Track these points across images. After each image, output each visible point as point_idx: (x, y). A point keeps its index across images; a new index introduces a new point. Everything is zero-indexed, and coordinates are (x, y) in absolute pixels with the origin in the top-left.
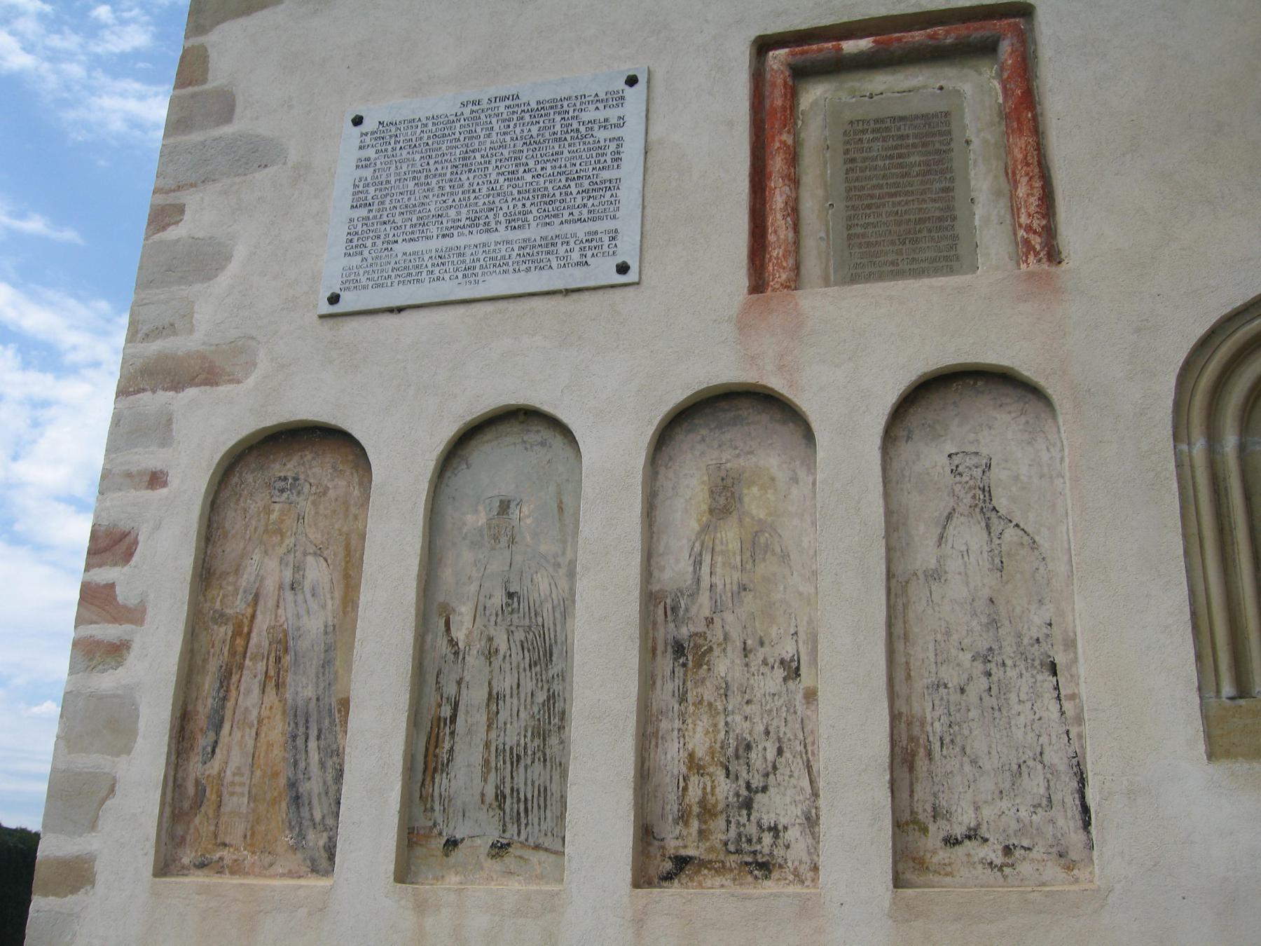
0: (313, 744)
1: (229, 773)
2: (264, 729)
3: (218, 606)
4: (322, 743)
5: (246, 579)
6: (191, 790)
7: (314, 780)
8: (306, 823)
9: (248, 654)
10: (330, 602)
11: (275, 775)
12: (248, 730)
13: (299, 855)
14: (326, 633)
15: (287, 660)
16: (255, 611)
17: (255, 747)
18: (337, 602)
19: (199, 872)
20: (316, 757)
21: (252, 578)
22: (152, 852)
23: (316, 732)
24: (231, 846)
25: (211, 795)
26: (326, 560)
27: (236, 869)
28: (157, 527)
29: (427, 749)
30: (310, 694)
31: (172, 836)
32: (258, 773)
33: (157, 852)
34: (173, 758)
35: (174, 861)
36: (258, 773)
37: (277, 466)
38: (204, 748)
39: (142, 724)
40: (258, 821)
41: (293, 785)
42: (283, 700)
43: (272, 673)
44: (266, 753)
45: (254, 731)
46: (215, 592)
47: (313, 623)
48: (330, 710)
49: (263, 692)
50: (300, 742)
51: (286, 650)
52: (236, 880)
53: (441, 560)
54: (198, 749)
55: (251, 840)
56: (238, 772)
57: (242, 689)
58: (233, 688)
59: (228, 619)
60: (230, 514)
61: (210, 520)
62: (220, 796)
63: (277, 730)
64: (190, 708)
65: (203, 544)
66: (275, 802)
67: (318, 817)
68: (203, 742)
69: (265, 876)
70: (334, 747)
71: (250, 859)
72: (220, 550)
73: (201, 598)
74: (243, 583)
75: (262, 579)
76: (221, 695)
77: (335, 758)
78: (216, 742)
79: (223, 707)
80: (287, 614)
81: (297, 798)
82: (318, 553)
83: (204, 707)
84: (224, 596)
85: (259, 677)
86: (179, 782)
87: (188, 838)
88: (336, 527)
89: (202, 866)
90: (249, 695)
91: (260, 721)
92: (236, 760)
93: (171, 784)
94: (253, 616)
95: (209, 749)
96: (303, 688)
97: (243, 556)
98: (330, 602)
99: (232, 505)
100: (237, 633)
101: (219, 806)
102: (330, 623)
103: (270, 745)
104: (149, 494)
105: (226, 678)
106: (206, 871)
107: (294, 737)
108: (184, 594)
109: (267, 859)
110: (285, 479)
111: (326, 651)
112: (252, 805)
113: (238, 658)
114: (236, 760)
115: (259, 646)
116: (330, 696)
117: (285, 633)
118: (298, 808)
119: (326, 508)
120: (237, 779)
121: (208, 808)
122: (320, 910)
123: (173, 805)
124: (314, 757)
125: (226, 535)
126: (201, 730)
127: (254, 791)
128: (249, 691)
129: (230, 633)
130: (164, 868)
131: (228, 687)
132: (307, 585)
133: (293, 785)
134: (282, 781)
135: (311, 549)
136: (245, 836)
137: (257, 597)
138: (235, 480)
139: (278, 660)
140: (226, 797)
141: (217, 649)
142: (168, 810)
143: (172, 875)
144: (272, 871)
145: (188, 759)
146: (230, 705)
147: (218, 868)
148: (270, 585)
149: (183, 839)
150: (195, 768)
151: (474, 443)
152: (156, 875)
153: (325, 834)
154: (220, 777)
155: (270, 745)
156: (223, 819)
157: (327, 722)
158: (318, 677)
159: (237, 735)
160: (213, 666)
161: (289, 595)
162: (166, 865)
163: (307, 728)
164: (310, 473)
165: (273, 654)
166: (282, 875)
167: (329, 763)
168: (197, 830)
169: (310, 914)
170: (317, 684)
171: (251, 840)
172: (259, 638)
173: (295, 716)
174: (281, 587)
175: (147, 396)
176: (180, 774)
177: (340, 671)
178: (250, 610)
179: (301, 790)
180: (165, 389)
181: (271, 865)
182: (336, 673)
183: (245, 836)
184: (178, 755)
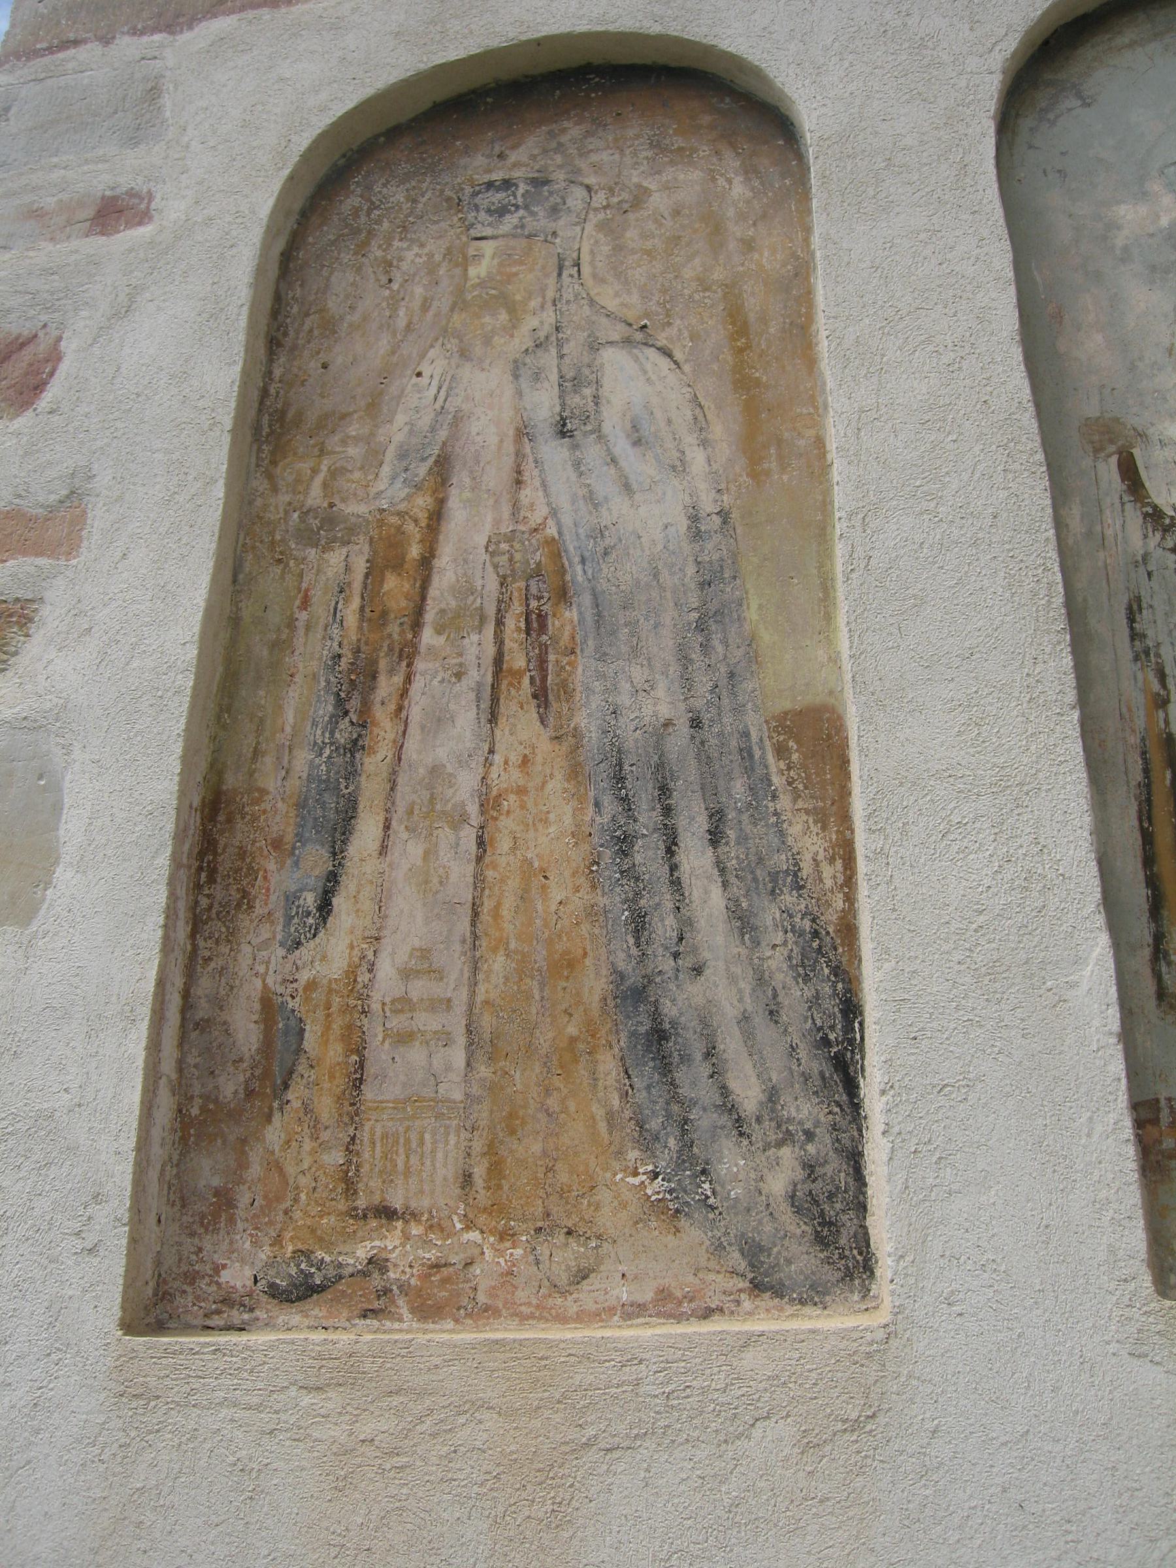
0: (696, 858)
1: (386, 970)
2: (507, 824)
3: (315, 496)
4: (732, 852)
5: (409, 416)
6: (246, 1032)
7: (715, 972)
8: (704, 1120)
9: (429, 616)
10: (697, 459)
11: (566, 965)
12: (445, 835)
13: (693, 1234)
14: (697, 535)
15: (566, 621)
16: (441, 502)
17: (479, 881)
18: (724, 450)
19: (292, 1316)
20: (717, 899)
21: (426, 420)
22: (118, 1241)
23: (702, 823)
24: (410, 1215)
25: (322, 1045)
26: (667, 353)
27: (439, 1296)
28: (124, 311)
29: (1147, 838)
30: (665, 711)
31: (180, 1194)
32: (499, 964)
33: (134, 1241)
34: (182, 931)
35: (191, 1278)
36: (499, 964)
37: (480, 160)
38: (291, 899)
39: (72, 829)
40: (512, 1123)
41: (635, 994)
42: (567, 737)
43: (517, 660)
44: (524, 897)
45: (468, 837)
46: (305, 466)
47: (644, 505)
48: (746, 753)
49: (493, 718)
50: (647, 855)
51: (563, 594)
52: (445, 1334)
53: (1059, 316)
54: (269, 901)
55: (492, 1192)
56: (423, 965)
57: (415, 713)
58: (382, 715)
59: (352, 530)
60: (342, 281)
61: (278, 298)
62: (358, 1048)
63: (554, 827)
64: (231, 781)
65: (262, 352)
66: (569, 1055)
67: (748, 1094)
68: (285, 879)
69: (562, 1319)
70: (781, 861)
71: (492, 1260)
72: (314, 365)
73: (260, 484)
74: (396, 430)
75: (458, 420)
76: (341, 738)
77: (788, 898)
78: (333, 879)
79: (352, 773)
80: (558, 489)
81: (659, 1035)
82: (640, 335)
83: (285, 775)
84: (334, 473)
85: (473, 675)
86: (203, 1010)
87: (244, 1199)
88: (688, 273)
89: (301, 1291)
90: (441, 727)
91: (489, 803)
92: (411, 925)
93: (175, 1001)
94: (437, 516)
95: (310, 900)
96: (637, 693)
97: (386, 374)
98: (697, 459)
99: (346, 257)
100: (387, 557)
101: (358, 1084)
102: (708, 504)
103: (535, 876)
104: (98, 243)
105: (353, 688)
106: (316, 1309)
107: (624, 843)
108: (213, 456)
109: (564, 1256)
110: (507, 184)
111: (704, 585)
112: (484, 1071)
113: (394, 629)
114: (411, 925)
115: (466, 590)
116: (738, 710)
117: (555, 548)
118: (665, 1068)
119: (645, 236)
120: (418, 989)
121: (316, 1089)
122: (855, 1426)
123: (181, 1088)
124: (709, 901)
125: (330, 327)
126: (277, 844)
127: (487, 1022)
128: (440, 720)
129: (360, 566)
130: (159, 1303)
131: (366, 708)
132: (612, 421)
133: (635, 994)
134: (594, 985)
135: (616, 332)
136: (467, 1179)
137: (443, 468)
138: (351, 201)
139: (535, 624)
140: (379, 1052)
141: (320, 609)
142: (166, 1101)
143: (187, 1329)
144: (587, 1296)
145: (231, 936)
146: (374, 764)
147: (372, 1292)
148: (487, 430)
149: (224, 1200)
150: (259, 961)
151: (1087, 52)
152: (129, 1326)
153: (786, 1153)
154: (355, 985)
155: (535, 876)
156: (373, 1127)
157: (739, 788)
158: (685, 660)
159: (409, 851)
160: (310, 655)
161: (554, 453)
162: (163, 1295)
163: (667, 811)
164: (582, 164)
165: (517, 608)
166: (633, 1311)
167: (769, 915)
168: (275, 1166)
169: (809, 1445)
170: (687, 682)
171: (492, 1192)
172: (465, 558)
173: (620, 779)
174: (524, 433)
175: (89, 53)
176: (205, 985)
177: (766, 637)
178: (423, 502)
179: (669, 1009)
180: (135, 32)
181: (583, 1275)
182: (751, 641)
183: (467, 1179)
184: (197, 925)
